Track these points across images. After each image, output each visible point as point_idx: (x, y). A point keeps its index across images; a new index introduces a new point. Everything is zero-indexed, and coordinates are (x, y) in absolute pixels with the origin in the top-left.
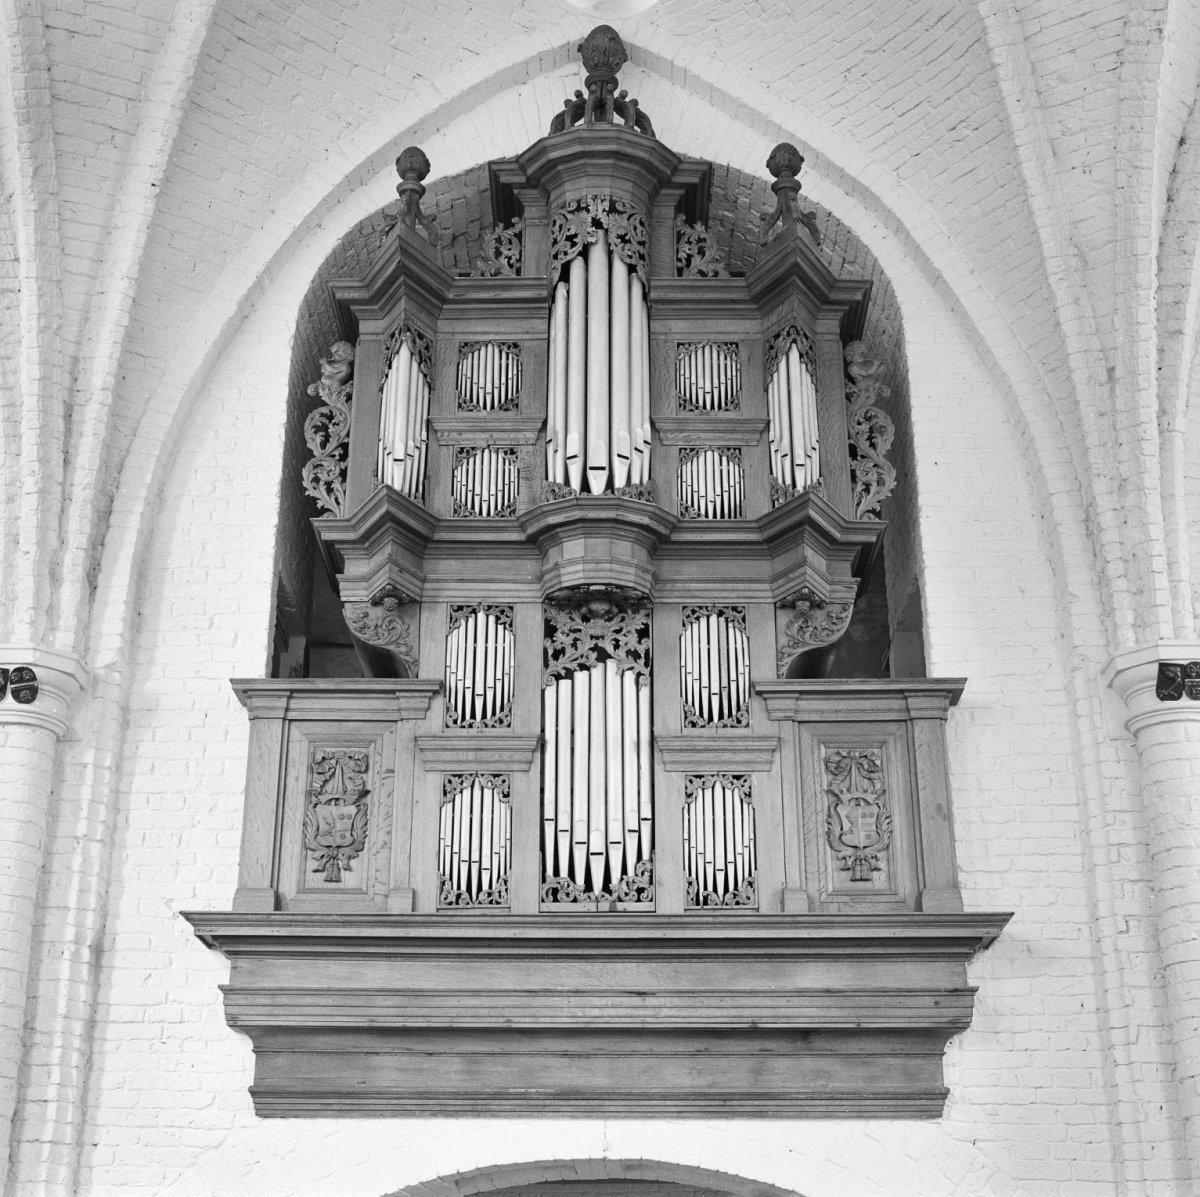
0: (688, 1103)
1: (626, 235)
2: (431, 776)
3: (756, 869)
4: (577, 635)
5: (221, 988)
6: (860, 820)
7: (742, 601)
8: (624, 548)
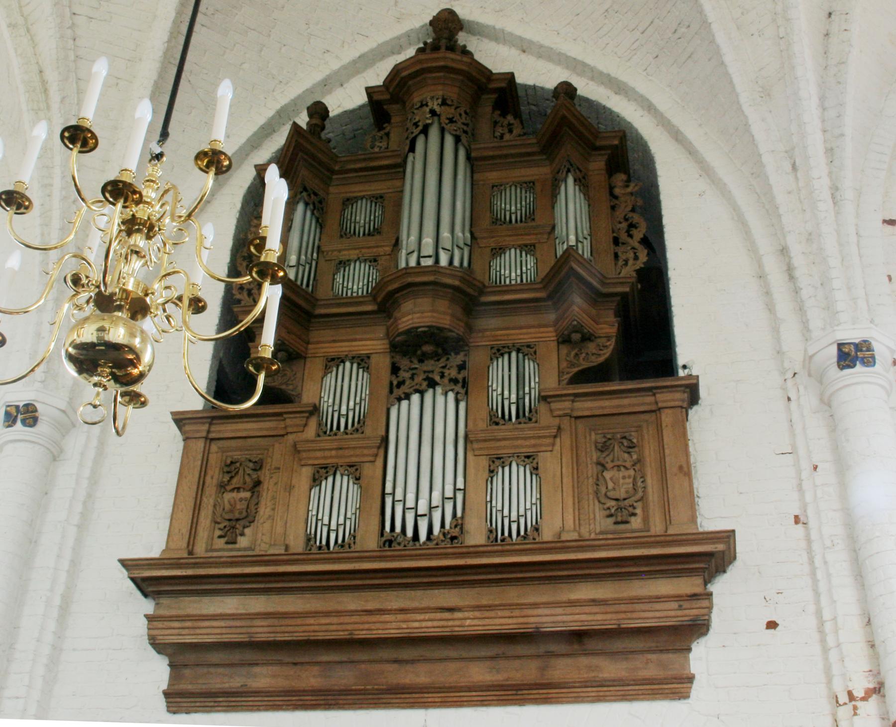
0: (489, 693)
1: (453, 118)
2: (304, 469)
3: (541, 518)
4: (414, 371)
5: (147, 616)
6: (621, 481)
7: (534, 340)
8: (443, 305)
